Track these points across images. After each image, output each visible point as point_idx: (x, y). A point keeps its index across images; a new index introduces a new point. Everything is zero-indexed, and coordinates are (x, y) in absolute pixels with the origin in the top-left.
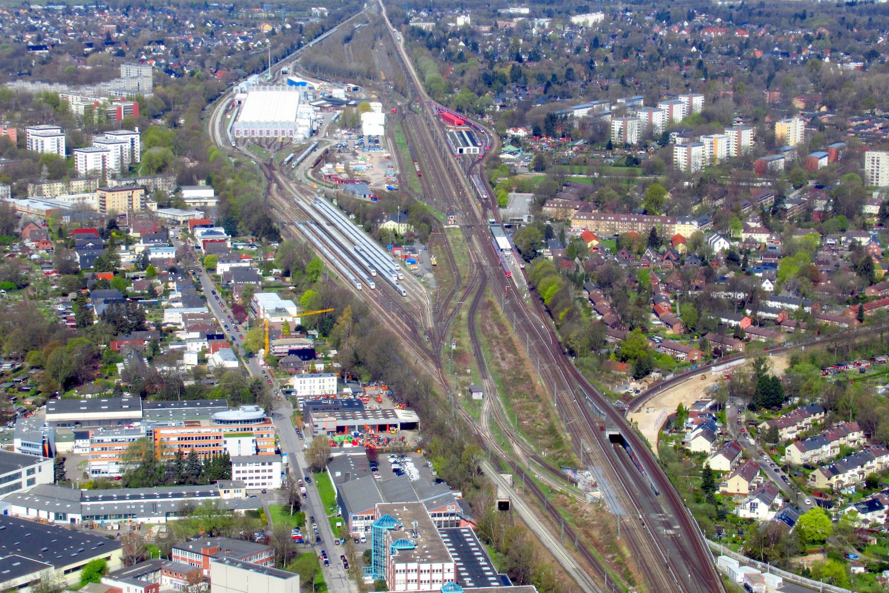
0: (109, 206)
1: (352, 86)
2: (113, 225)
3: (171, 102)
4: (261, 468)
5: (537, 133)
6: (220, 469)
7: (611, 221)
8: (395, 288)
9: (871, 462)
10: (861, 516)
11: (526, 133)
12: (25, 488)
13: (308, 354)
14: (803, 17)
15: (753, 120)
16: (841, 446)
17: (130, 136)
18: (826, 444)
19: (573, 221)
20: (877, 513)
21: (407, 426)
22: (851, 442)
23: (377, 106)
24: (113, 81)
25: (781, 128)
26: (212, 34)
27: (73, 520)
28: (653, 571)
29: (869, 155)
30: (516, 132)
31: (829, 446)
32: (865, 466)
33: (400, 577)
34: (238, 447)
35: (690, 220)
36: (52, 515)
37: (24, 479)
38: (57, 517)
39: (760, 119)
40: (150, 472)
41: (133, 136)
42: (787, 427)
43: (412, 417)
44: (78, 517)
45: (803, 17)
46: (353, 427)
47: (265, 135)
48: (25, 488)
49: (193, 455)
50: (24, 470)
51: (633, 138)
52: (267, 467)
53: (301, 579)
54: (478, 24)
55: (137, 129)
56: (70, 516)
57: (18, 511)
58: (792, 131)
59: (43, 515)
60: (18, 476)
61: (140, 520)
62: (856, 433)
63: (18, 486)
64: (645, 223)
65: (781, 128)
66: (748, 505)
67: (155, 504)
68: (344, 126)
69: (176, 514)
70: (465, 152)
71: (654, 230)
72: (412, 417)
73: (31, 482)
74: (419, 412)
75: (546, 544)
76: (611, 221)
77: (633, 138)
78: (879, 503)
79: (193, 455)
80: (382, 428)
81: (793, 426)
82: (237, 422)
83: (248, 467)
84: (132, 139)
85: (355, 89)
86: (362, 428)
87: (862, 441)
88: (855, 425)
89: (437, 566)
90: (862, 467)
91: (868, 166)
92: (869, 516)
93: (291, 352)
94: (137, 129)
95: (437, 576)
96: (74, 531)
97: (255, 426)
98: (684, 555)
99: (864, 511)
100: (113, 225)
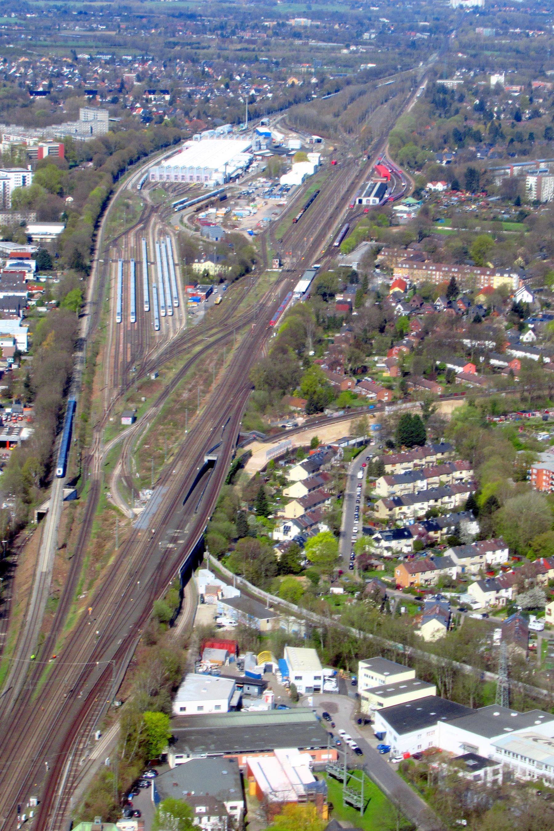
1: (316, 137)
3: (113, 147)
7: (432, 270)
9: (450, 497)
10: (384, 544)
11: (445, 187)
16: (441, 483)
17: (22, 174)
18: (422, 479)
19: (396, 270)
20: (404, 541)
22: (457, 480)
24: (64, 125)
26: (435, 74)
28: (116, 578)
30: (435, 185)
31: (425, 482)
32: (440, 500)
35: (509, 273)
41: (25, 174)
42: (401, 463)
47: (173, 180)
55: (29, 167)
62: (464, 472)
64: (443, 271)
66: (282, 528)
70: (364, 202)
71: (453, 279)
75: (42, 546)
76: (432, 270)
78: (409, 532)
81: (409, 462)
84: (24, 177)
85: (319, 141)
90: (436, 501)
92: (394, 544)
94: (29, 167)
98: (161, 566)
99: (387, 538)
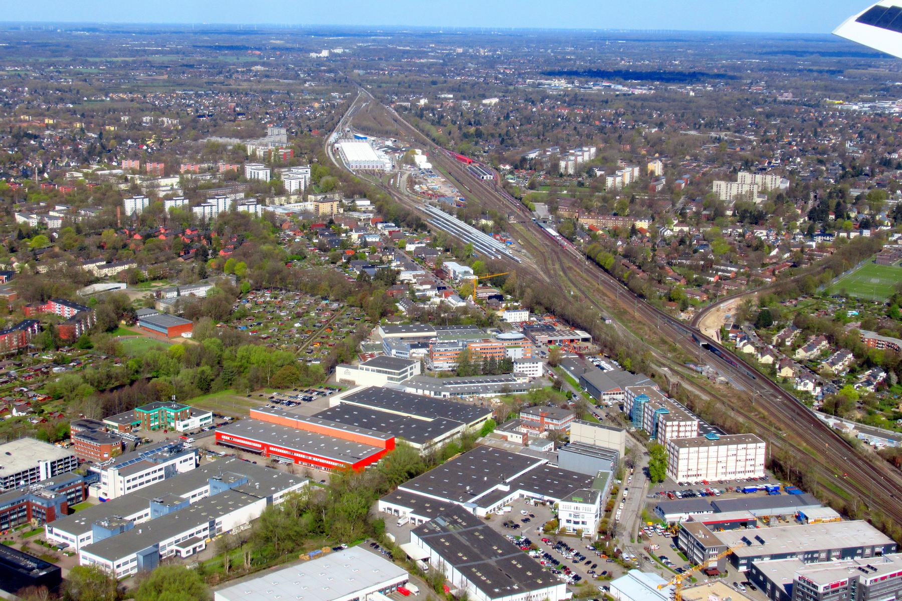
0: (321, 211)
2: (331, 222)
4: (532, 365)
5: (516, 168)
6: (507, 366)
8: (513, 259)
12: (409, 378)
13: (500, 298)
14: (607, 102)
15: (639, 163)
21: (585, 340)
23: (419, 151)
25: (651, 166)
27: (444, 396)
29: (715, 183)
33: (668, 429)
34: (514, 354)
36: (432, 393)
37: (408, 373)
38: (435, 394)
39: (642, 163)
40: (465, 369)
43: (587, 335)
44: (448, 394)
45: (607, 102)
46: (556, 341)
48: (409, 378)
49: (493, 358)
50: (408, 368)
51: (571, 171)
52: (535, 365)
53: (767, 448)
54: (432, 103)
56: (443, 393)
57: (410, 390)
58: (657, 167)
59: (427, 393)
60: (406, 371)
61: (481, 395)
63: (406, 377)
65: (651, 166)
67: (486, 386)
68: (407, 163)
69: (499, 392)
72: (587, 335)
73: (411, 374)
74: (590, 333)
77: (571, 171)
79: (493, 358)
80: (572, 341)
82: (510, 340)
83: (526, 365)
86: (561, 341)
87: (828, 346)
88: (823, 337)
89: (689, 423)
91: (715, 189)
93: (490, 297)
95: (689, 428)
96: (446, 401)
97: (520, 342)
100: (331, 222)
